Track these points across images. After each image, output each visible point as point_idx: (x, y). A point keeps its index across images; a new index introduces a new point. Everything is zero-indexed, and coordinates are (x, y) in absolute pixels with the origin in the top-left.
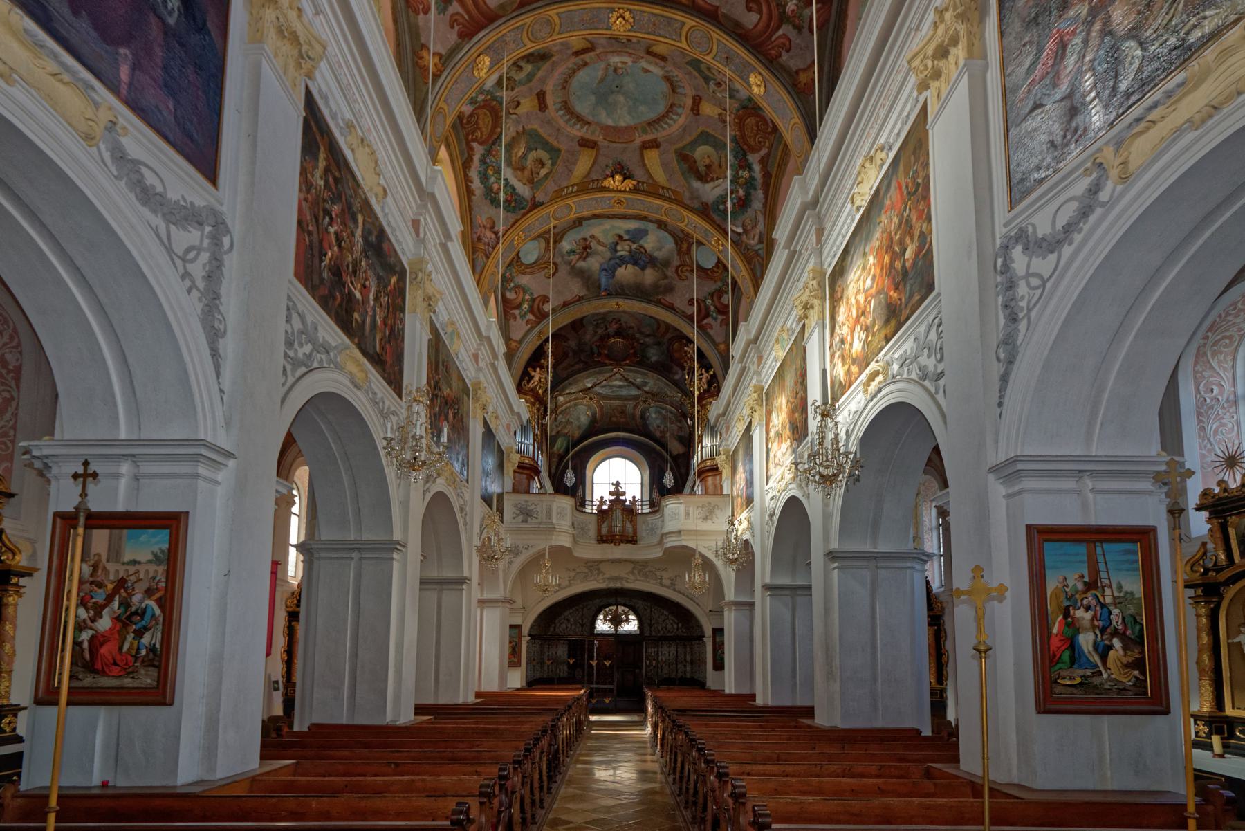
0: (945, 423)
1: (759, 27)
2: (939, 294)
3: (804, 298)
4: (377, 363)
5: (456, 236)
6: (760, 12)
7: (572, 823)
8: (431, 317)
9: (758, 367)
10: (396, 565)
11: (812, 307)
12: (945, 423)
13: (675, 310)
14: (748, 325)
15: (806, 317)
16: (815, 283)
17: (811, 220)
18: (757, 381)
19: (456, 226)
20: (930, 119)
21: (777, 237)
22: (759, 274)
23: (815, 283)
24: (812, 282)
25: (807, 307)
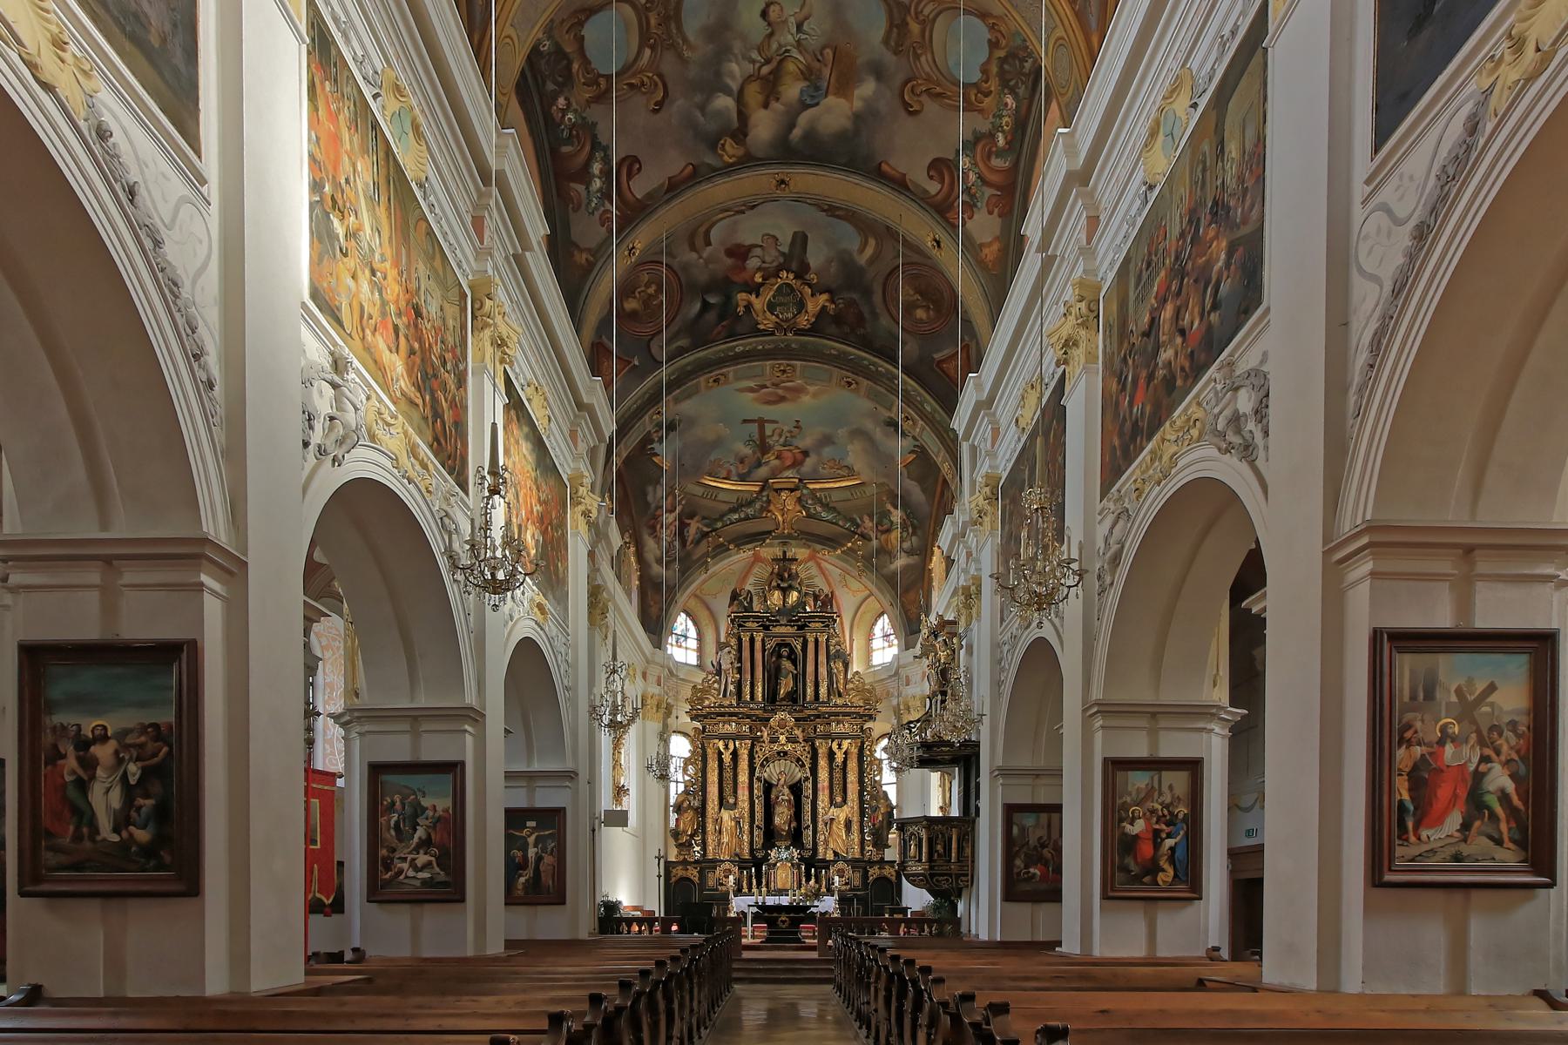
0: (1267, 499)
1: (939, 197)
2: (1268, 310)
3: (1064, 333)
4: (320, 240)
5: (539, 243)
6: (942, 181)
7: (200, 157)
8: (505, 368)
9: (993, 446)
10: (469, 739)
11: (1076, 344)
12: (1267, 499)
13: (908, 189)
14: (980, 377)
15: (1066, 362)
16: (1083, 305)
17: (1080, 203)
18: (990, 467)
19: (537, 228)
20: (1271, 28)
21: (1028, 233)
22: (1093, 21)
23: (1083, 305)
24: (1079, 305)
25: (1069, 344)
